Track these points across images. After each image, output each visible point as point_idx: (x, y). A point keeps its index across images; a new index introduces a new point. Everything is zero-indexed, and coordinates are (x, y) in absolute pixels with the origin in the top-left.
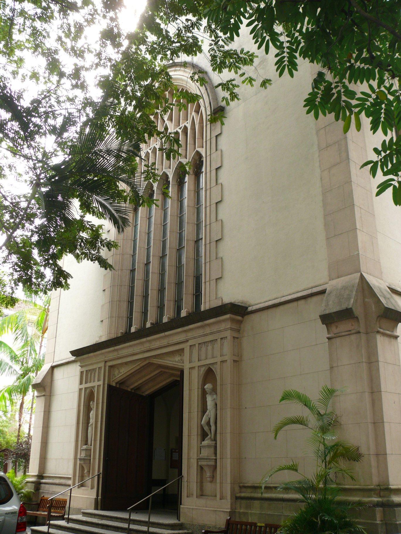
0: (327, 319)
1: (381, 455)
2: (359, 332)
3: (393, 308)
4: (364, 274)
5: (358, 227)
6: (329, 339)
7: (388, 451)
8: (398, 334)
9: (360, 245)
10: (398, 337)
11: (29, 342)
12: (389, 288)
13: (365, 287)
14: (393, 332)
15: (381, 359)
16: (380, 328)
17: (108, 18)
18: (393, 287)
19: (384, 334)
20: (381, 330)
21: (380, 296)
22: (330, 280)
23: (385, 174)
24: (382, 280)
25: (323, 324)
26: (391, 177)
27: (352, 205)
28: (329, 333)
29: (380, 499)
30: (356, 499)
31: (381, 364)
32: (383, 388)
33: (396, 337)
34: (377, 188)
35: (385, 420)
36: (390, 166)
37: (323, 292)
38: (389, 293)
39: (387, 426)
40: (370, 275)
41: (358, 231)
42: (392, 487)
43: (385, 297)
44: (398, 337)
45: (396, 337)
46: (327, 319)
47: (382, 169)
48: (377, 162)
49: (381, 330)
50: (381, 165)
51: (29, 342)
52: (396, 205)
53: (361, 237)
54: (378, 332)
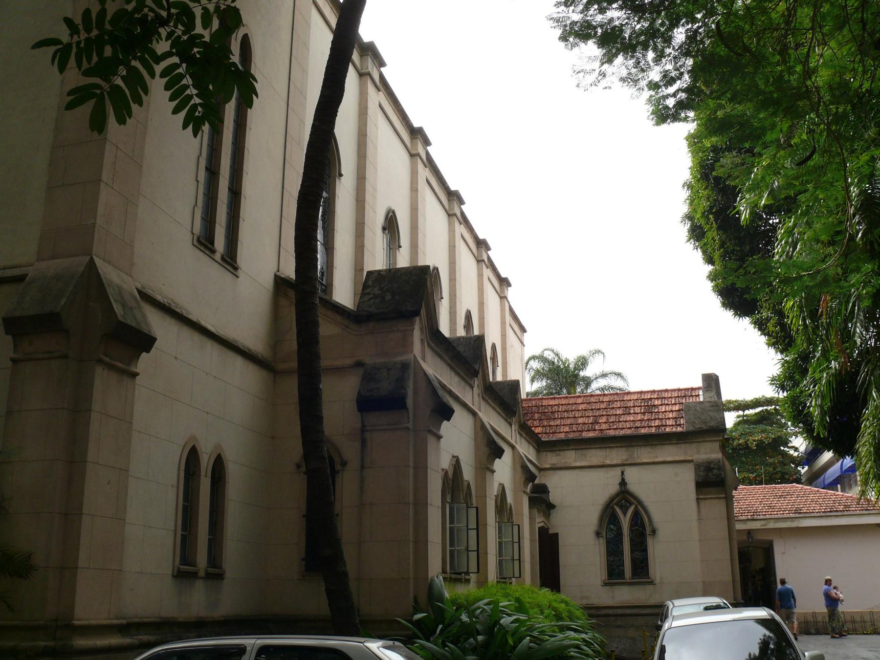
0: (17, 327)
1: (68, 568)
2: (64, 357)
3: (134, 325)
4: (96, 260)
5: (104, 178)
6: (13, 360)
7: (82, 562)
8: (138, 371)
9: (101, 209)
10: (138, 374)
11: (458, 576)
12: (139, 292)
13: (91, 282)
14: (129, 365)
15: (96, 406)
16: (106, 355)
17: (643, 83)
18: (150, 292)
19: (111, 367)
20: (107, 359)
21: (116, 301)
22: (38, 260)
23: (86, 73)
24: (131, 276)
25: (7, 333)
26: (97, 80)
27: (364, 236)
28: (15, 351)
29: (52, 644)
30: (9, 644)
31: (94, 416)
32: (91, 455)
33: (134, 375)
34: (69, 94)
35: (85, 511)
36: (95, 59)
37: (20, 279)
38: (136, 299)
39: (86, 521)
40: (109, 263)
41: (102, 185)
42: (76, 622)
43: (124, 305)
44: (138, 374)
45: (134, 375)
46: (17, 327)
47: (79, 64)
48: (69, 46)
49: (107, 359)
50: (76, 54)
51: (458, 576)
52: (92, 130)
53: (106, 197)
54: (100, 361)
